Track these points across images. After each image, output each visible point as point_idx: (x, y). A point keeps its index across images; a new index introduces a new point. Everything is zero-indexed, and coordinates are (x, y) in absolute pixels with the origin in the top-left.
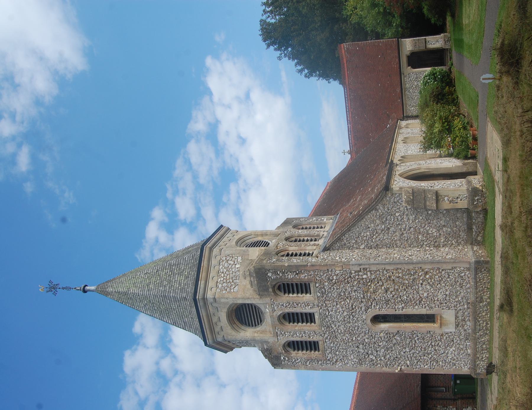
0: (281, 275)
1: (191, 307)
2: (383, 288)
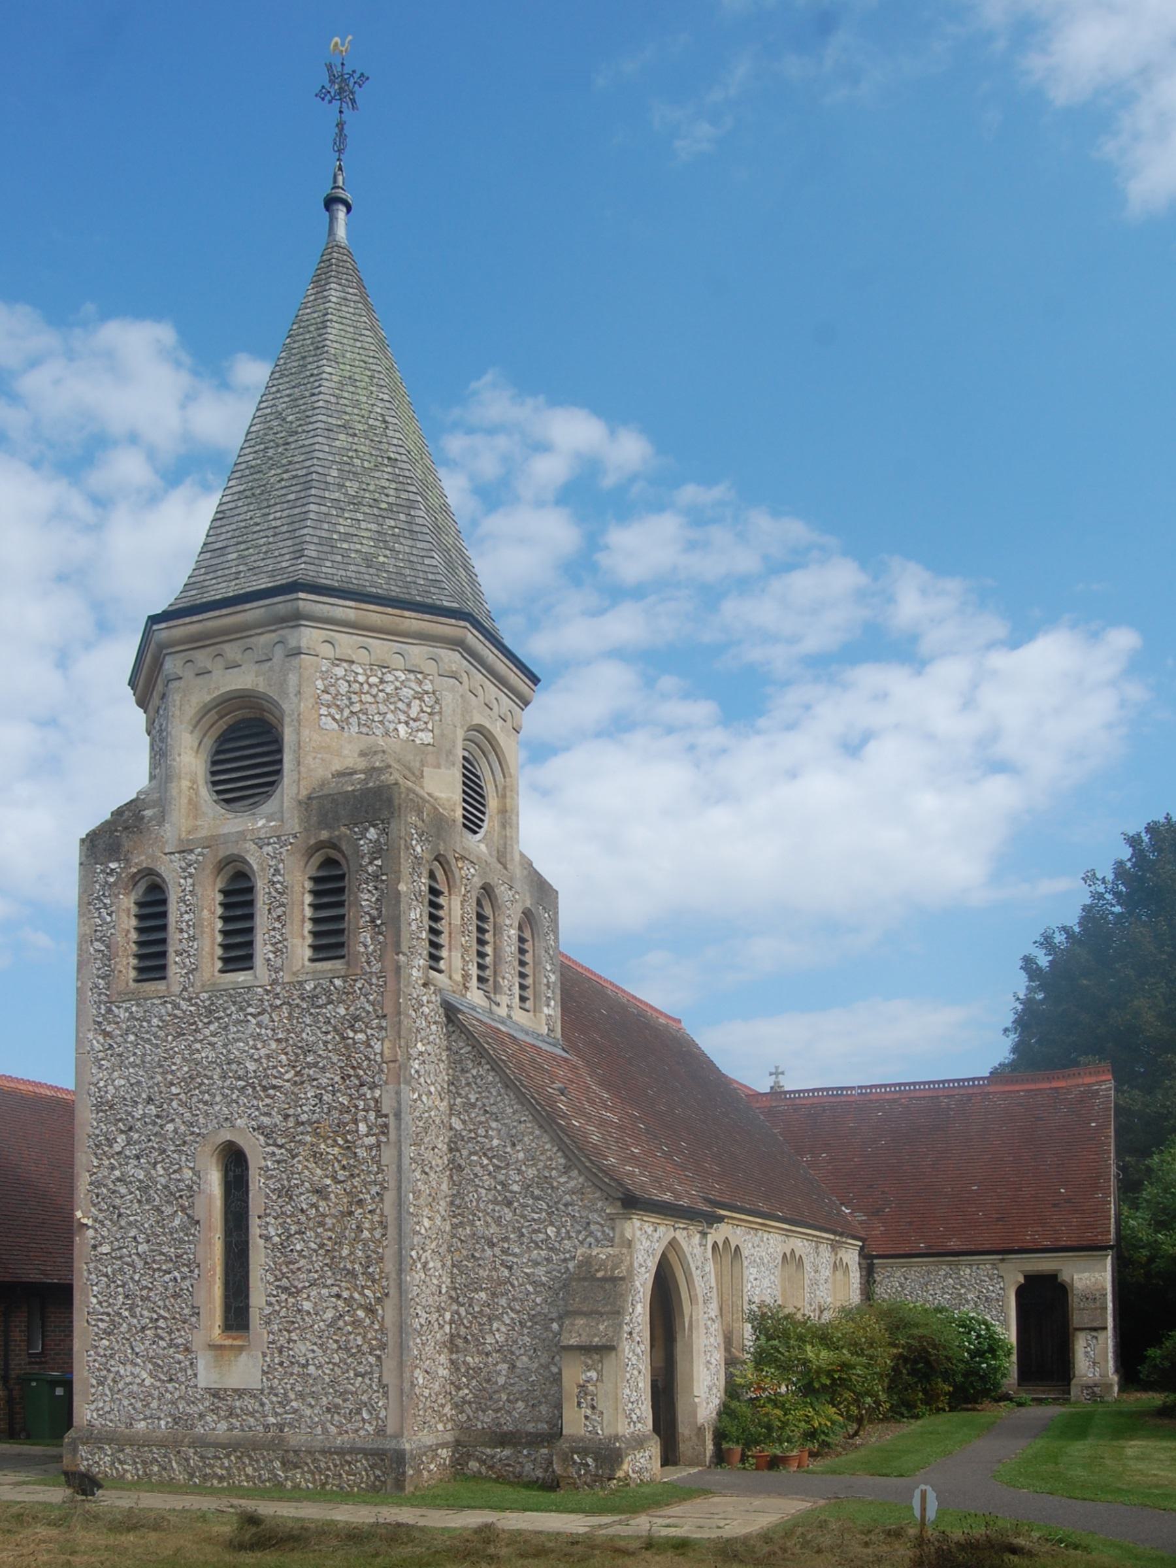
0: (370, 869)
1: (272, 574)
2: (328, 1181)
